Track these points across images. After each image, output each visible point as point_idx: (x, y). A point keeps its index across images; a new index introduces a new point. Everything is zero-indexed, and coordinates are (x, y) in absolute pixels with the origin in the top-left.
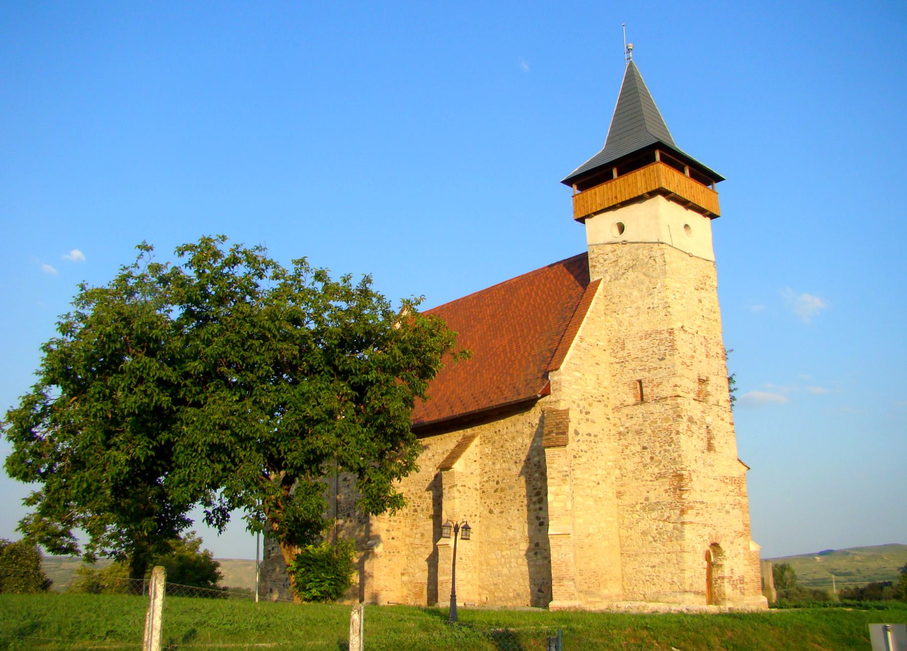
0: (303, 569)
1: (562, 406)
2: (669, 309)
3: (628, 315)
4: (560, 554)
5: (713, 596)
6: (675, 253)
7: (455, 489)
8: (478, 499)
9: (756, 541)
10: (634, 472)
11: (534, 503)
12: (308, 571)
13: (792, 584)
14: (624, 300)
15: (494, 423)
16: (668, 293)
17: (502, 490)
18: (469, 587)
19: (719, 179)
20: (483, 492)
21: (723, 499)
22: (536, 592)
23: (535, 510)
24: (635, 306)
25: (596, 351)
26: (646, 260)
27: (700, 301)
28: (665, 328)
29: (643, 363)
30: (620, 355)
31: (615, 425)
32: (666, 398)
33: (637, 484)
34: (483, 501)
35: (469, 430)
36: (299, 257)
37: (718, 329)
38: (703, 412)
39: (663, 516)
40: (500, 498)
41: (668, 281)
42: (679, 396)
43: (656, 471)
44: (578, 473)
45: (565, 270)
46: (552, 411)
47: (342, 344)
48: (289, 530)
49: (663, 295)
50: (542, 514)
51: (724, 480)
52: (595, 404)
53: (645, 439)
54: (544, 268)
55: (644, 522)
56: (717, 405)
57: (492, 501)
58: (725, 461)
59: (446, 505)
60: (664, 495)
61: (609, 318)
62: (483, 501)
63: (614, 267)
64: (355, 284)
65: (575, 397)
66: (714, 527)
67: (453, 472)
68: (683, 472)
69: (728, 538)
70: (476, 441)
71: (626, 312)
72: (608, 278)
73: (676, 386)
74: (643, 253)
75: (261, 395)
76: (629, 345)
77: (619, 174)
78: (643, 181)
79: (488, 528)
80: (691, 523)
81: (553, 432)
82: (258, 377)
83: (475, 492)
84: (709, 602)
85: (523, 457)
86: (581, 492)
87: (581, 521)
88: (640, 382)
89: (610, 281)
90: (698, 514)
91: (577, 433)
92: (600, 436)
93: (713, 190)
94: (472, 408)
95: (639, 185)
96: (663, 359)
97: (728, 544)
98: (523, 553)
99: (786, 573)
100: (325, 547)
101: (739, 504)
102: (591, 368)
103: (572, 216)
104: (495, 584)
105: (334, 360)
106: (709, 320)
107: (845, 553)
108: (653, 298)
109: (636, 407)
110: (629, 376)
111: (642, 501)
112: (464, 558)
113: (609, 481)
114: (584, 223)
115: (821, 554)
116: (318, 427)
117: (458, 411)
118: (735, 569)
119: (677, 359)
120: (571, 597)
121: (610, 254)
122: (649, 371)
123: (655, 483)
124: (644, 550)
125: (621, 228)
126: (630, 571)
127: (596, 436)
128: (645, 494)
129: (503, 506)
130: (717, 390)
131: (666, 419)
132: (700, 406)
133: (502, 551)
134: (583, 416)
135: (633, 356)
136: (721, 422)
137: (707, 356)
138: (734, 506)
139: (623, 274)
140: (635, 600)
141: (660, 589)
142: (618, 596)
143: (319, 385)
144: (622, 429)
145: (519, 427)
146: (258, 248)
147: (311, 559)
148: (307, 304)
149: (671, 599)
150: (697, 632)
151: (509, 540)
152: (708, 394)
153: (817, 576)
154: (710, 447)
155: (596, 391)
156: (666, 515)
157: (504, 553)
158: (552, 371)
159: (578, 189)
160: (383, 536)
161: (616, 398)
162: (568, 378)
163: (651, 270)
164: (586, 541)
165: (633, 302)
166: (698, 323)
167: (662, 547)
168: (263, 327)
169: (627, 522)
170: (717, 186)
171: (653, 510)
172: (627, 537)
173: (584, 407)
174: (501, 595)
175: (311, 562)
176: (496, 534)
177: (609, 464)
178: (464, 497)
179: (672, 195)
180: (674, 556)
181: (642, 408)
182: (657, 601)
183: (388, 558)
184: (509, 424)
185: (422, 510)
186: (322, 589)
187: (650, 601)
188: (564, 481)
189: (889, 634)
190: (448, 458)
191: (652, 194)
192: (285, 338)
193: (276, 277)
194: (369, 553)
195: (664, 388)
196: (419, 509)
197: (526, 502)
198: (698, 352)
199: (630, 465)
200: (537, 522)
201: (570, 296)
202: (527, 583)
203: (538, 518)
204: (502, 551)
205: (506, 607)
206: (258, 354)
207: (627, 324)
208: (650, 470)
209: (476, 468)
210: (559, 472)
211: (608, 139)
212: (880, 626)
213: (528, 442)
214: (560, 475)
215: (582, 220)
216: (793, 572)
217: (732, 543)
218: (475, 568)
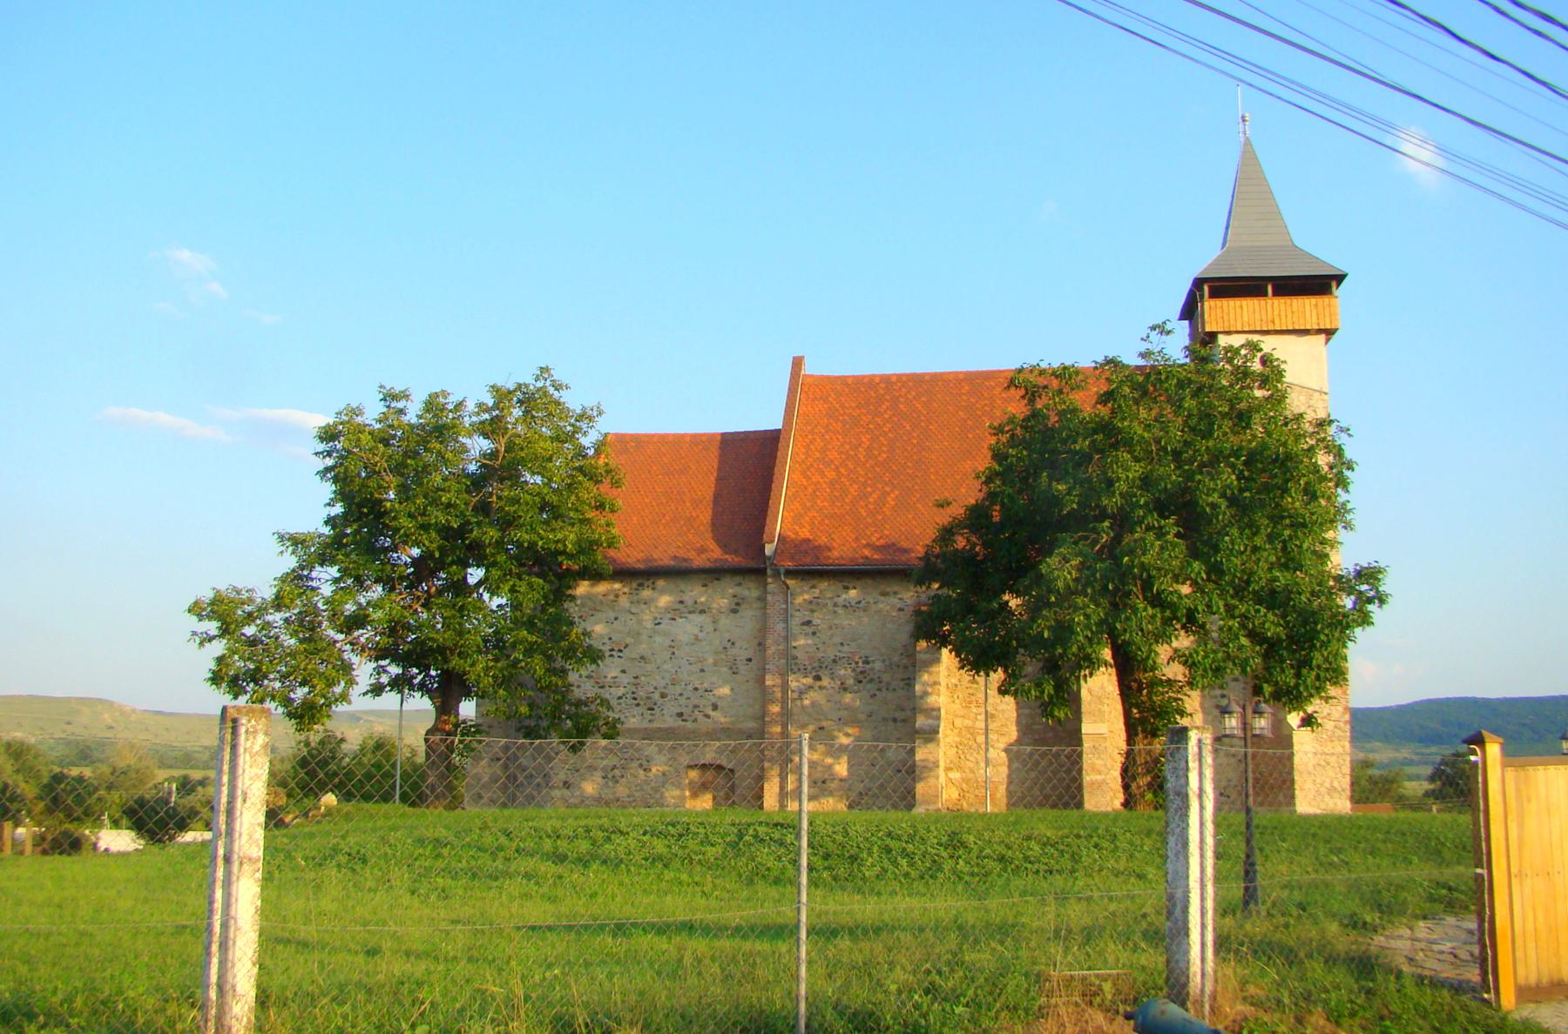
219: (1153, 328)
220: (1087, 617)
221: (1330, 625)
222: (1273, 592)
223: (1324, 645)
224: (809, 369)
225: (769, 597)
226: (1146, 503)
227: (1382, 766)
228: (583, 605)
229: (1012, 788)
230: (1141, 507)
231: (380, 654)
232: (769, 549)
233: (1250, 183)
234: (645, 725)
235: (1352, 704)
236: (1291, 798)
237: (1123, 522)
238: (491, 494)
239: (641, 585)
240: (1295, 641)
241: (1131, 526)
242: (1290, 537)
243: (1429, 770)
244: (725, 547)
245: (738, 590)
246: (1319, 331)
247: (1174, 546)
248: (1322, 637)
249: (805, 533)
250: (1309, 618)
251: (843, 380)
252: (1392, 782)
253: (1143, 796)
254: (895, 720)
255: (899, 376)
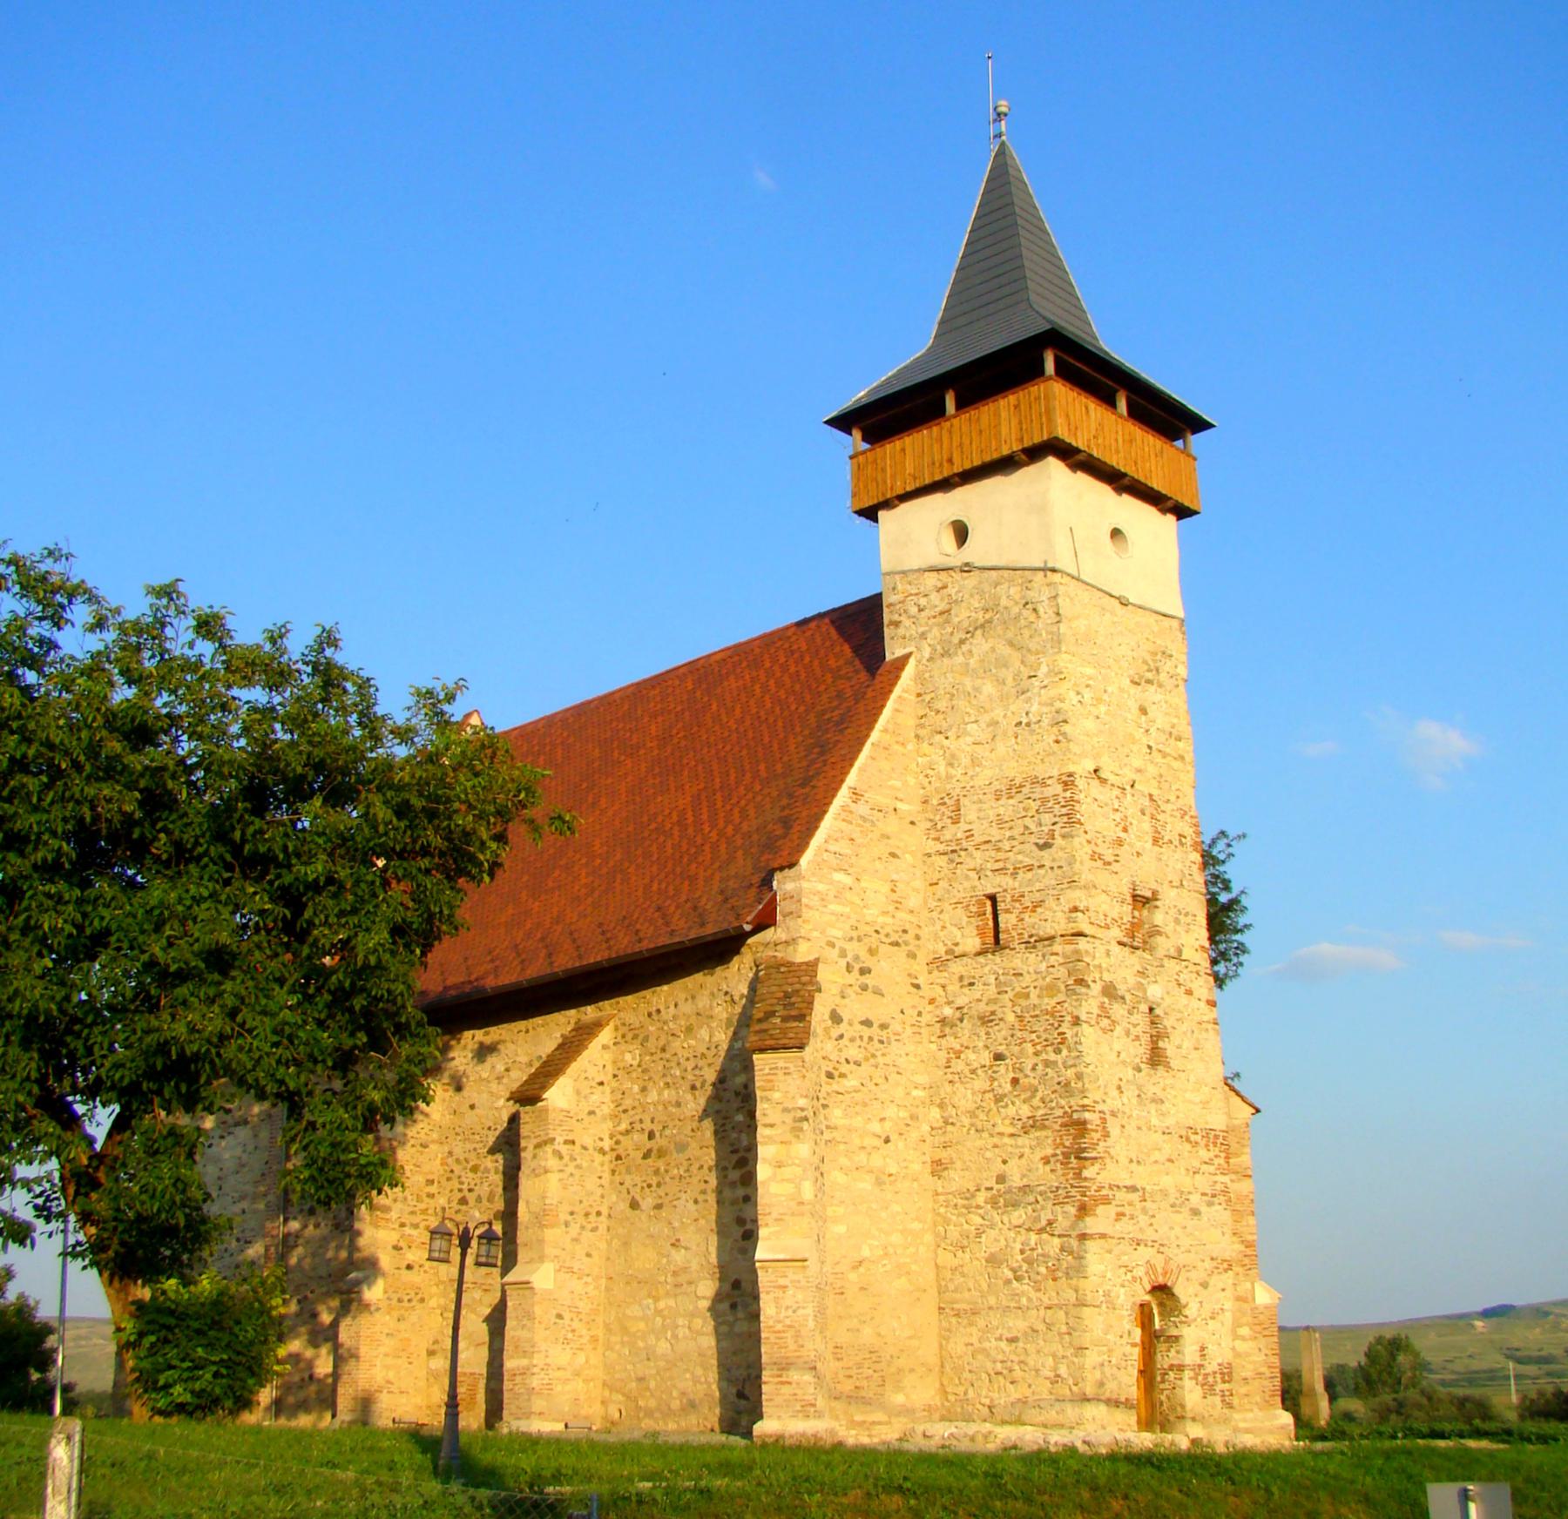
0: (153, 1338)
1: (802, 953)
2: (1066, 728)
3: (969, 740)
4: (781, 1307)
5: (1155, 1414)
6: (1085, 595)
7: (549, 1149)
8: (607, 1175)
9: (1272, 1283)
10: (973, 1114)
11: (733, 1184)
12: (166, 1341)
13: (1414, 1383)
14: (961, 703)
15: (647, 993)
16: (1064, 689)
17: (661, 1153)
18: (579, 1385)
19: (1199, 425)
20: (618, 1158)
21: (1187, 1182)
22: (733, 1398)
23: (734, 1202)
24: (986, 718)
25: (891, 825)
26: (1016, 610)
27: (1143, 711)
28: (1055, 773)
29: (1001, 855)
30: (947, 835)
31: (932, 1001)
32: (1051, 938)
33: (979, 1143)
34: (617, 1178)
35: (589, 1009)
36: (163, 579)
37: (1186, 779)
38: (1141, 973)
39: (1038, 1219)
40: (657, 1172)
41: (1063, 660)
42: (1080, 934)
43: (1025, 1111)
44: (836, 1115)
45: (833, 632)
46: (778, 966)
47: (257, 796)
48: (123, 1243)
49: (1052, 692)
50: (747, 1215)
51: (1188, 1135)
52: (884, 949)
53: (1000, 1036)
54: (787, 628)
55: (993, 1233)
56: (1178, 956)
57: (638, 1180)
58: (1194, 1092)
59: (527, 1186)
60: (1043, 1170)
61: (925, 747)
62: (617, 1178)
63: (941, 626)
64: (297, 646)
65: (836, 933)
66: (1160, 1247)
67: (545, 1110)
68: (1087, 1115)
69: (1193, 1275)
70: (606, 1036)
71: (966, 733)
72: (927, 652)
73: (1075, 909)
74: (1008, 594)
75: (42, 909)
76: (970, 812)
77: (961, 405)
78: (1014, 422)
79: (625, 1244)
80: (1103, 1236)
81: (778, 1016)
82: (35, 867)
83: (599, 1158)
84: (1147, 1424)
85: (711, 1075)
86: (843, 1161)
87: (841, 1229)
88: (993, 898)
89: (931, 659)
90: (1120, 1215)
91: (836, 1018)
92: (895, 1026)
93: (1185, 451)
94: (597, 955)
95: (1004, 431)
96: (1046, 846)
97: (1193, 1288)
98: (706, 1304)
99: (1401, 1358)
100: (206, 1285)
101: (1225, 1192)
102: (878, 864)
103: (847, 504)
104: (641, 1379)
105: (233, 829)
106: (1165, 755)
107: (1539, 1313)
108: (1028, 700)
109: (981, 959)
110: (967, 884)
111: (992, 1183)
112: (567, 1316)
113: (914, 1135)
114: (876, 520)
115: (1487, 1314)
116: (182, 991)
117: (565, 962)
118: (1211, 1349)
119: (1080, 847)
120: (808, 1409)
121: (934, 597)
122: (1014, 875)
123: (1020, 1141)
124: (992, 1301)
125: (961, 533)
126: (960, 1349)
127: (883, 1026)
128: (998, 1167)
129: (661, 1192)
130: (1177, 921)
131: (1051, 989)
132: (1134, 960)
133: (656, 1299)
134: (854, 977)
135: (978, 839)
136: (1184, 999)
137: (1155, 841)
138: (1211, 1197)
139: (962, 642)
140: (968, 1419)
141: (1028, 1392)
142: (929, 1409)
143: (193, 889)
144: (948, 1011)
145: (703, 1002)
146: (51, 553)
147: (172, 1313)
148: (173, 692)
149: (1052, 1415)
150: (1029, 1500)
151: (675, 1273)
152: (1155, 932)
153: (1476, 1365)
154: (1156, 1058)
155: (889, 920)
156: (1045, 1216)
157: (662, 1305)
158: (781, 869)
159: (864, 439)
160: (385, 1260)
161: (936, 937)
162: (821, 887)
163: (1026, 633)
164: (853, 1276)
165: (982, 709)
166: (1137, 763)
167: (1033, 1294)
168: (51, 746)
169: (954, 1233)
170: (1196, 441)
171: (1015, 1205)
172: (954, 1270)
173: (857, 958)
174: (652, 1403)
175: (172, 1321)
176: (645, 1258)
177: (915, 1093)
178: (571, 1169)
179: (1081, 457)
181: (995, 962)
182: (1019, 1422)
183: (396, 1314)
184: (682, 996)
185: (479, 1200)
186: (198, 1386)
187: (1004, 1422)
188: (797, 1131)
189: (1472, 1507)
190: (533, 1078)
191: (1034, 453)
192: (110, 770)
193: (99, 624)
194: (350, 1301)
195: (1048, 914)
196: (471, 1197)
197: (713, 1182)
198: (1133, 830)
199: (965, 1097)
201: (839, 695)
202: (713, 1376)
203: (741, 1221)
204: (656, 1299)
205: (655, 1434)
206: (36, 809)
207: (965, 761)
208: (1011, 1111)
209: (602, 1099)
210: (786, 1110)
211: (942, 322)
212: (1452, 1489)
213: (723, 1038)
214: (788, 1118)
215: (870, 513)
216: (1417, 1355)
217: (1205, 1285)
218: (594, 1339)
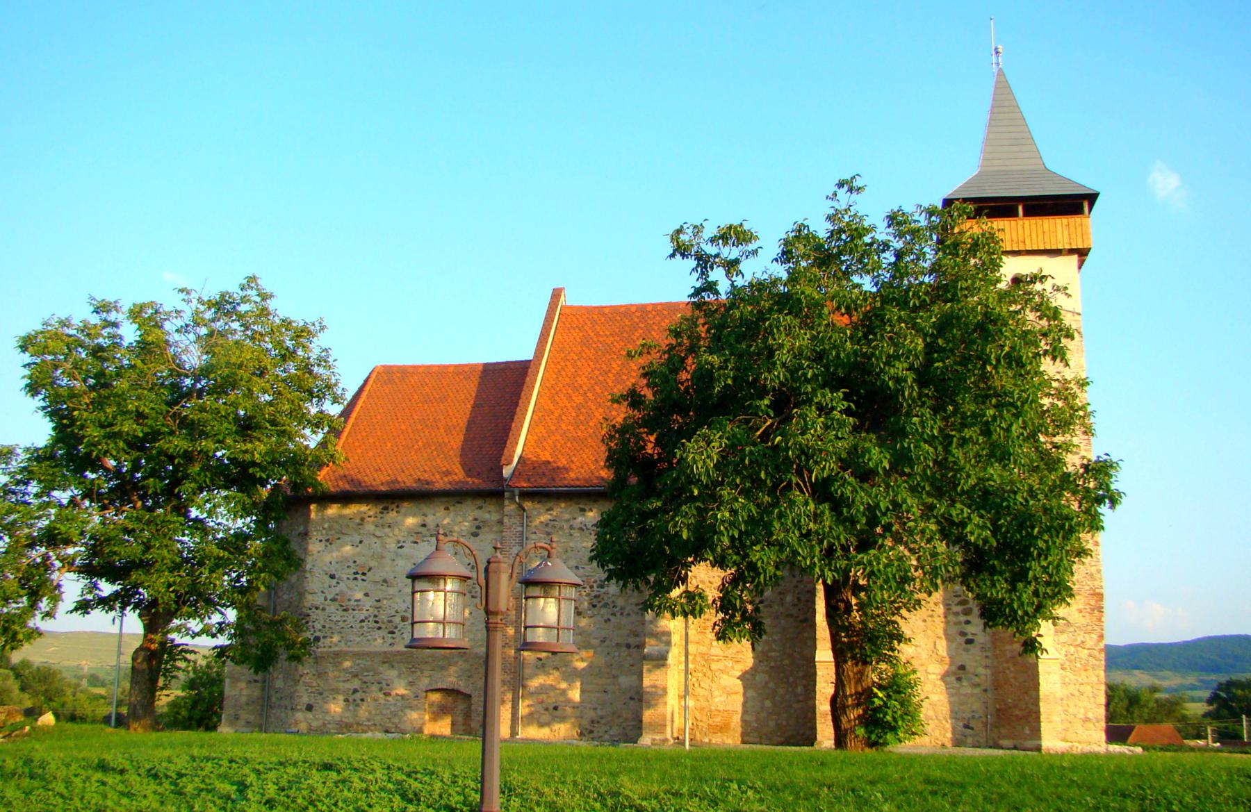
11: (956, 614)
180: (1089, 688)
200: (962, 640)
219: (841, 185)
220: (733, 512)
221: (1048, 529)
222: (986, 493)
223: (1043, 553)
224: (571, 299)
225: (506, 520)
226: (815, 376)
227: (1166, 690)
228: (330, 528)
229: (747, 717)
230: (807, 381)
231: (88, 570)
232: (507, 472)
233: (1004, 110)
234: (387, 649)
235: (1119, 636)
236: (1036, 732)
237: (785, 402)
238: (799, 516)
239: (386, 508)
240: (1017, 552)
241: (839, 427)
242: (994, 418)
243: (1206, 694)
244: (469, 471)
245: (478, 513)
246: (1071, 252)
247: (841, 424)
248: (1041, 544)
249: (546, 456)
250: (1024, 520)
251: (600, 309)
252: (1177, 704)
253: (853, 731)
254: (628, 646)
255: (655, 305)
